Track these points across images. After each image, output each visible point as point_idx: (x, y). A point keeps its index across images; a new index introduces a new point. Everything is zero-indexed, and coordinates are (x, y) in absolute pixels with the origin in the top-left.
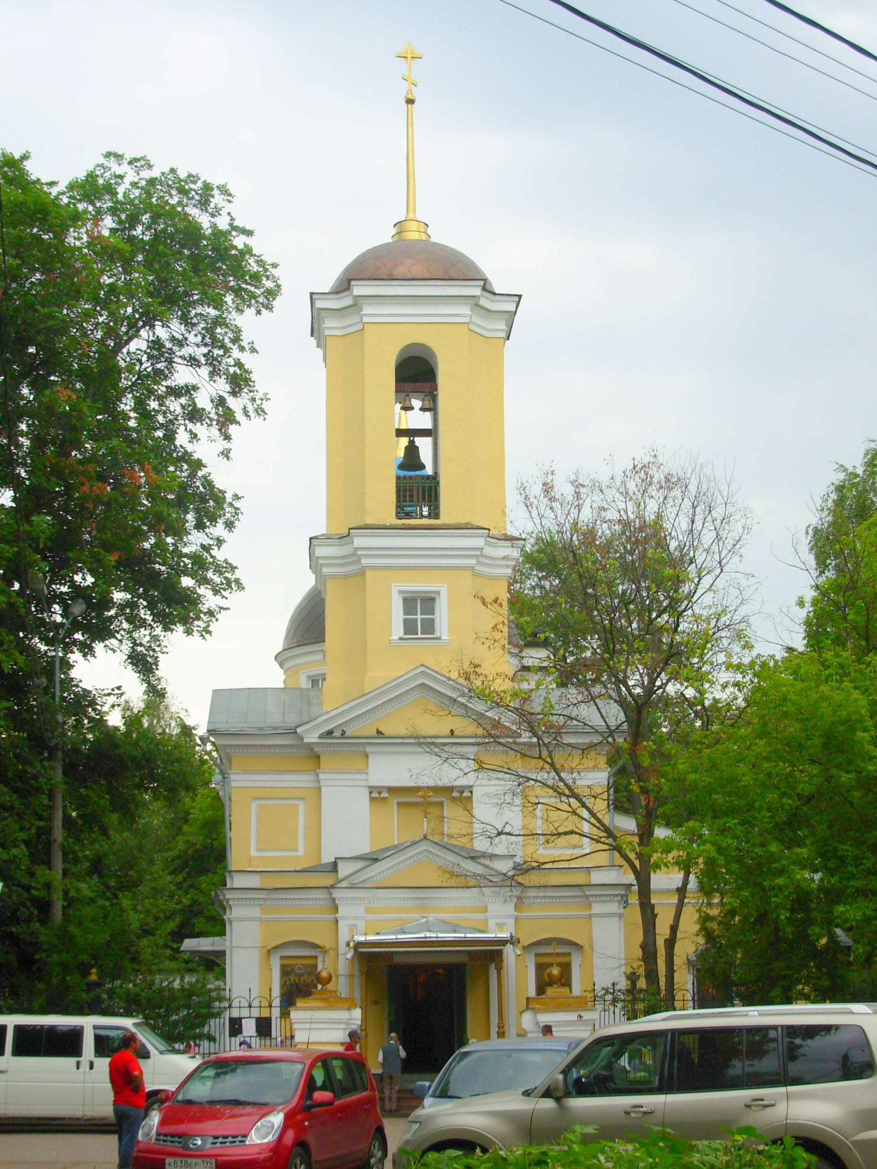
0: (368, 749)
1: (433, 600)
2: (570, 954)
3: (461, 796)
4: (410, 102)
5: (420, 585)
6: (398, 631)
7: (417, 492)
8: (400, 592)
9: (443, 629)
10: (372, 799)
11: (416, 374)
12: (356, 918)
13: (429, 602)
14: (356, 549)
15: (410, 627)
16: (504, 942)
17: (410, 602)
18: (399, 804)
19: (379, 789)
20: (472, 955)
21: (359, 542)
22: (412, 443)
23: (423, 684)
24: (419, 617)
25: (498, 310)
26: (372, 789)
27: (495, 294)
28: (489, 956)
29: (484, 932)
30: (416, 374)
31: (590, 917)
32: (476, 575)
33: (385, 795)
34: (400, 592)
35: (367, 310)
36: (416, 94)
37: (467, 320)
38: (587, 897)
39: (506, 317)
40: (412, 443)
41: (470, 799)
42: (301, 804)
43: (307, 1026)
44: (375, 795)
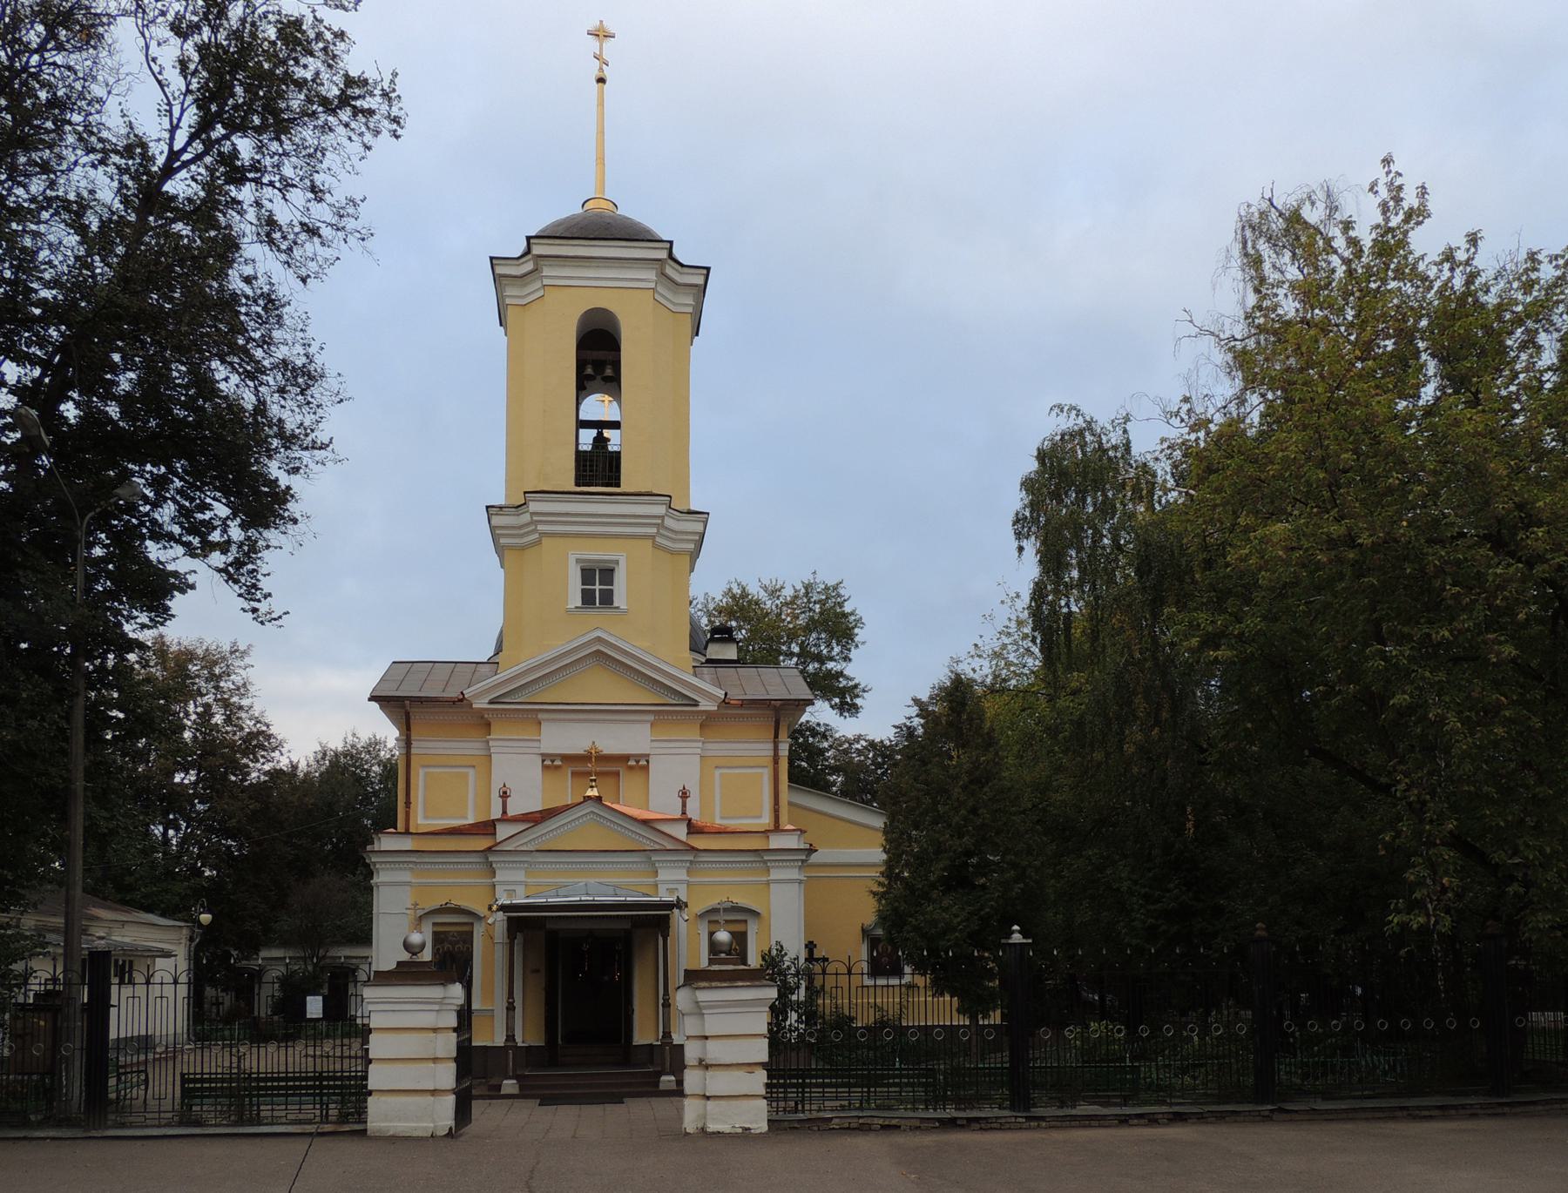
0: (540, 716)
1: (612, 570)
2: (746, 921)
3: (637, 765)
4: (601, 80)
5: (597, 553)
6: (577, 601)
7: (598, 468)
8: (578, 561)
9: (619, 600)
10: (545, 768)
11: (598, 355)
12: (515, 883)
13: (608, 574)
14: (533, 514)
15: (588, 598)
16: (669, 906)
17: (587, 575)
18: (574, 774)
19: (552, 757)
20: (638, 922)
21: (533, 507)
22: (600, 434)
23: (598, 652)
24: (597, 587)
25: (687, 286)
26: (544, 757)
27: (682, 265)
28: (653, 922)
29: (425, 809)
30: (598, 355)
31: (768, 883)
32: (656, 546)
33: (558, 763)
34: (578, 561)
35: (546, 272)
36: (608, 73)
37: (652, 285)
38: (765, 862)
39: (695, 290)
40: (600, 434)
41: (646, 768)
42: (471, 772)
43: (436, 1007)
44: (548, 762)
